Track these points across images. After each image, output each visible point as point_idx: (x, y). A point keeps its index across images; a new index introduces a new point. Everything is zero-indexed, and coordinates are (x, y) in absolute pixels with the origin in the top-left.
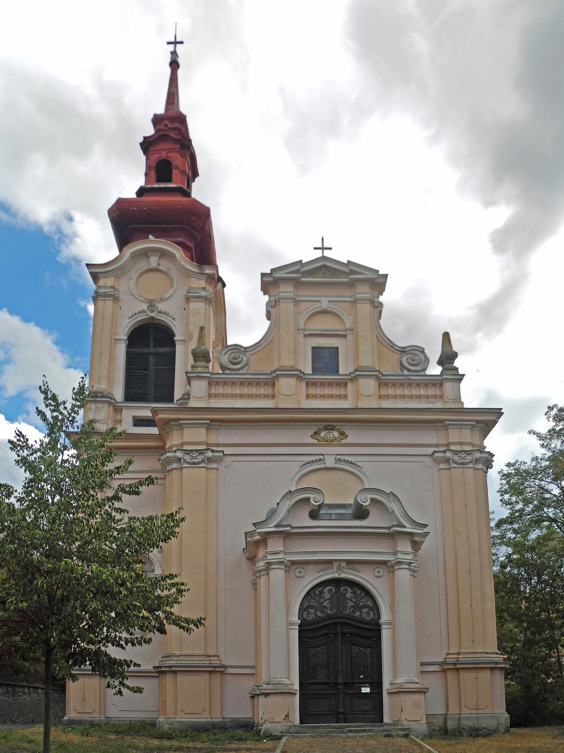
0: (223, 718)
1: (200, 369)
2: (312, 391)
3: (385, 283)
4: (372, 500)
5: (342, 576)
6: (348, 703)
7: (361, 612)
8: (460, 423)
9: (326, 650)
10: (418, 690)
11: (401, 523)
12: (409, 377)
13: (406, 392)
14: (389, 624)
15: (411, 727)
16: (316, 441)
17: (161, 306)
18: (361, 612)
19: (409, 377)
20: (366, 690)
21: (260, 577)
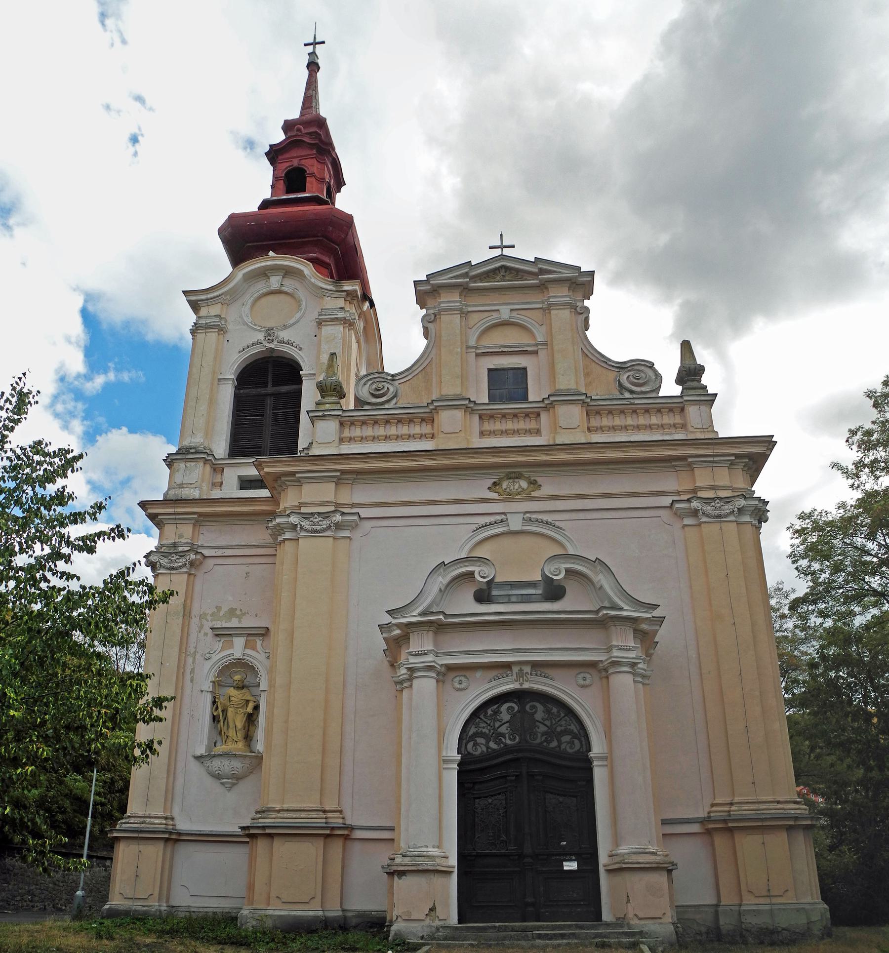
0: (343, 911)
1: (327, 406)
2: (487, 426)
3: (592, 282)
4: (568, 571)
5: (526, 686)
6: (542, 888)
7: (559, 741)
8: (711, 459)
9: (504, 802)
10: (654, 865)
12: (632, 401)
13: (630, 421)
14: (604, 758)
15: (645, 929)
16: (495, 495)
17: (284, 335)
18: (559, 741)
19: (632, 401)
20: (571, 866)
21: (402, 690)
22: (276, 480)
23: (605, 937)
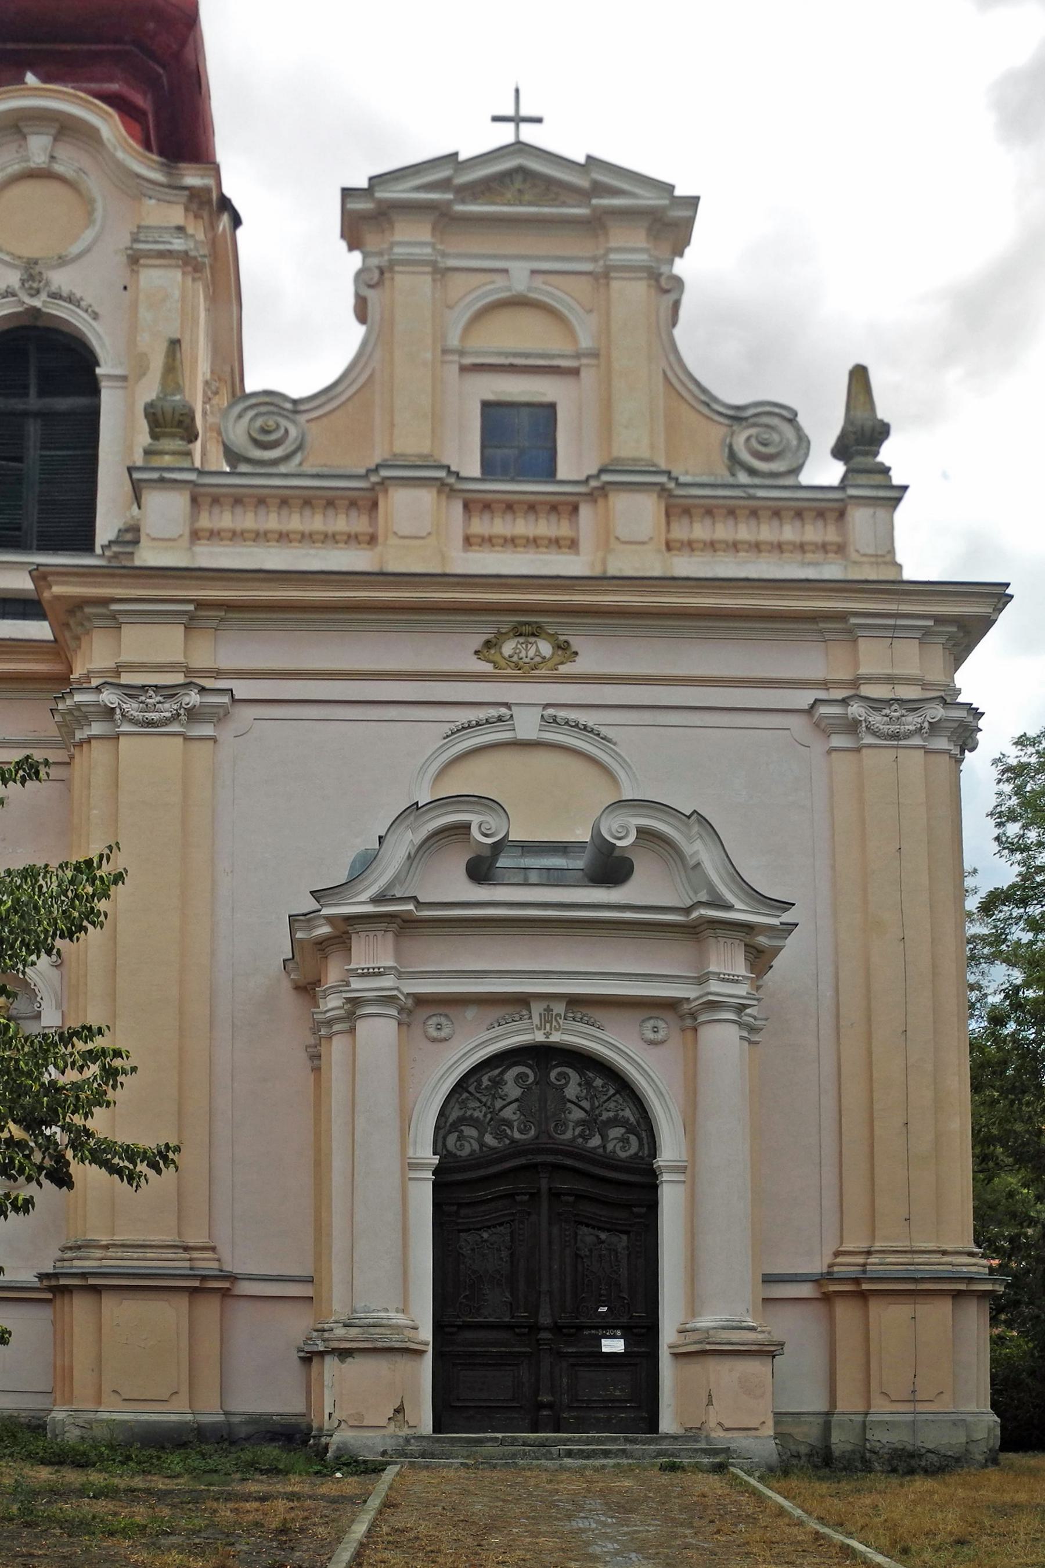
0: (226, 1414)
1: (167, 460)
2: (480, 526)
4: (642, 831)
5: (556, 1038)
7: (604, 1137)
8: (891, 622)
9: (508, 1238)
10: (754, 1348)
11: (720, 897)
12: (752, 491)
14: (681, 1170)
15: (733, 1446)
16: (487, 668)
17: (60, 279)
18: (604, 1137)
19: (752, 491)
20: (613, 1345)
22: (71, 612)
23: (672, 1455)
